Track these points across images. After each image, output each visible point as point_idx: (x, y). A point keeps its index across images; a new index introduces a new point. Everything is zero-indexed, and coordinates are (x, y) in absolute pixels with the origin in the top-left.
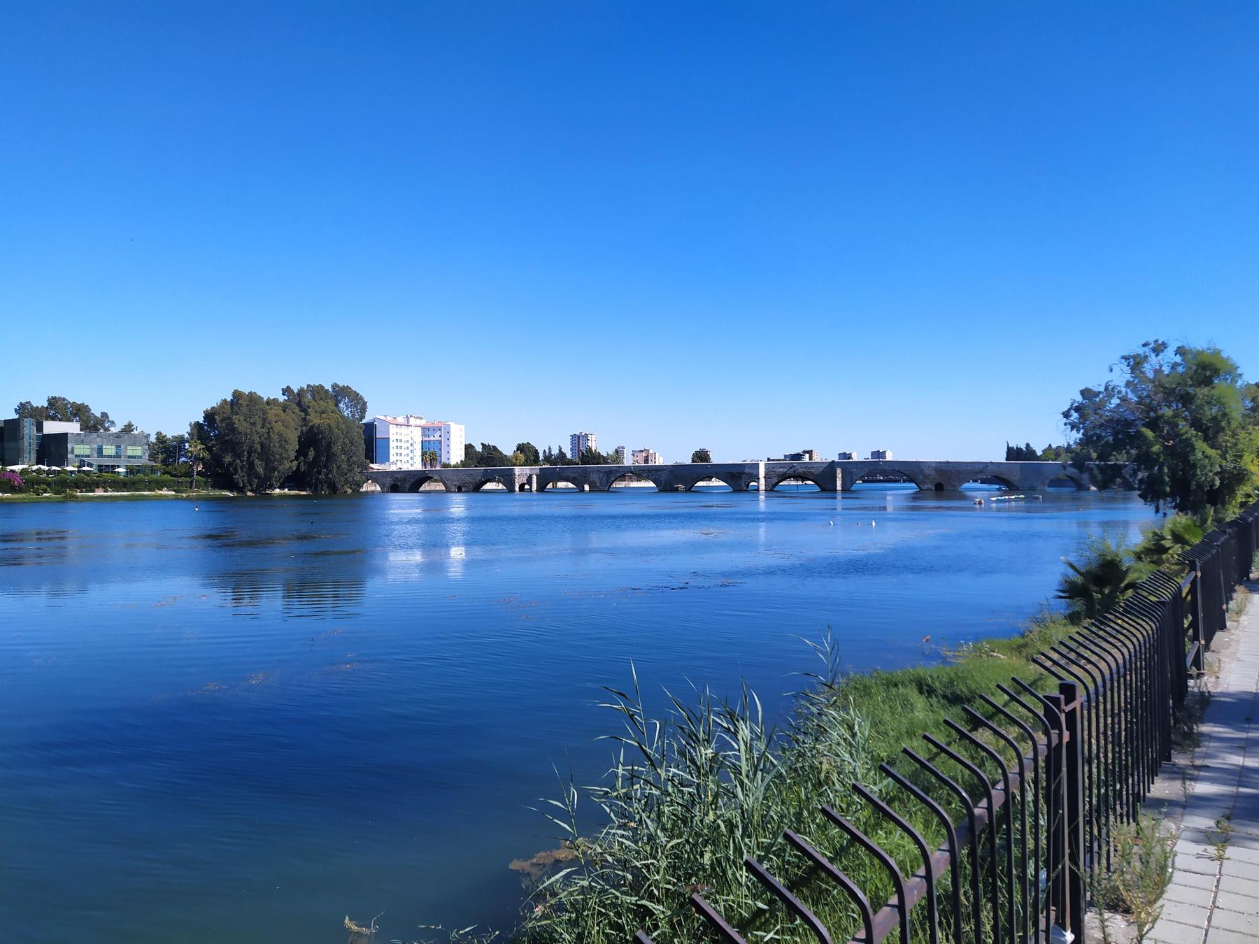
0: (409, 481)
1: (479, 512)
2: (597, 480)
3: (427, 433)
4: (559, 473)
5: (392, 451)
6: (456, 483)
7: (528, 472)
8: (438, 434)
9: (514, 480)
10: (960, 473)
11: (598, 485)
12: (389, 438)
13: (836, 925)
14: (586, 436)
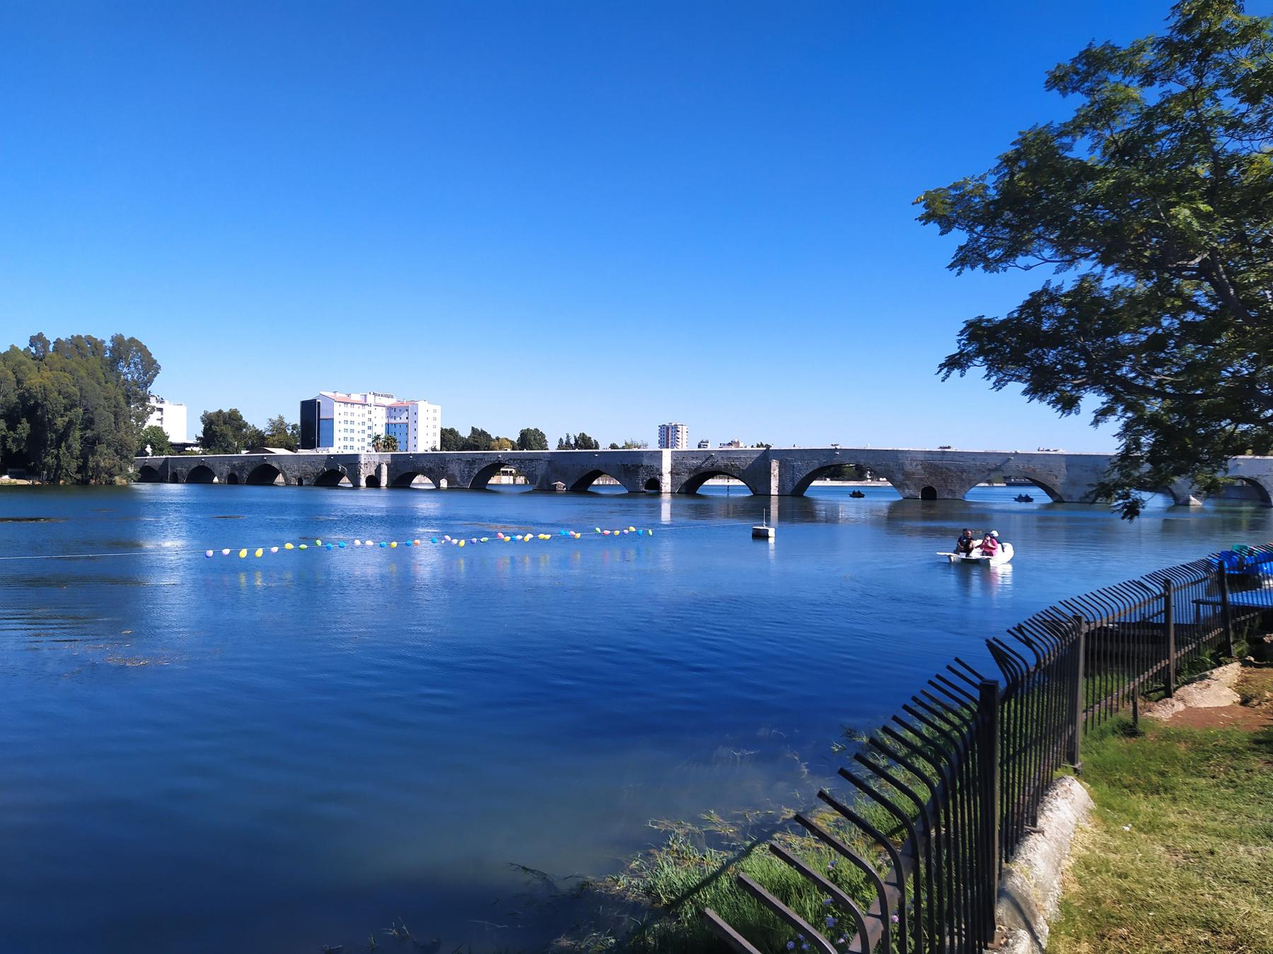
0: (247, 470)
1: (1055, 500)
2: (457, 473)
3: (393, 414)
4: (413, 462)
5: (337, 435)
6: (296, 473)
7: (377, 460)
8: (404, 415)
9: (360, 471)
10: (963, 471)
11: (458, 479)
12: (333, 419)
13: (831, 874)
14: (676, 426)
